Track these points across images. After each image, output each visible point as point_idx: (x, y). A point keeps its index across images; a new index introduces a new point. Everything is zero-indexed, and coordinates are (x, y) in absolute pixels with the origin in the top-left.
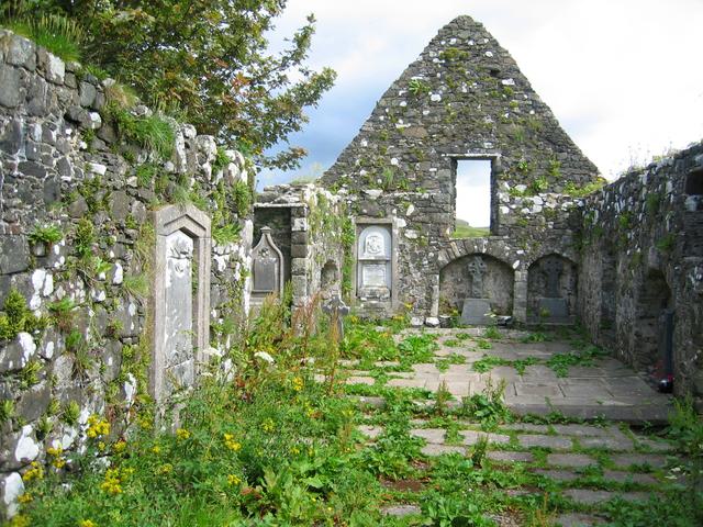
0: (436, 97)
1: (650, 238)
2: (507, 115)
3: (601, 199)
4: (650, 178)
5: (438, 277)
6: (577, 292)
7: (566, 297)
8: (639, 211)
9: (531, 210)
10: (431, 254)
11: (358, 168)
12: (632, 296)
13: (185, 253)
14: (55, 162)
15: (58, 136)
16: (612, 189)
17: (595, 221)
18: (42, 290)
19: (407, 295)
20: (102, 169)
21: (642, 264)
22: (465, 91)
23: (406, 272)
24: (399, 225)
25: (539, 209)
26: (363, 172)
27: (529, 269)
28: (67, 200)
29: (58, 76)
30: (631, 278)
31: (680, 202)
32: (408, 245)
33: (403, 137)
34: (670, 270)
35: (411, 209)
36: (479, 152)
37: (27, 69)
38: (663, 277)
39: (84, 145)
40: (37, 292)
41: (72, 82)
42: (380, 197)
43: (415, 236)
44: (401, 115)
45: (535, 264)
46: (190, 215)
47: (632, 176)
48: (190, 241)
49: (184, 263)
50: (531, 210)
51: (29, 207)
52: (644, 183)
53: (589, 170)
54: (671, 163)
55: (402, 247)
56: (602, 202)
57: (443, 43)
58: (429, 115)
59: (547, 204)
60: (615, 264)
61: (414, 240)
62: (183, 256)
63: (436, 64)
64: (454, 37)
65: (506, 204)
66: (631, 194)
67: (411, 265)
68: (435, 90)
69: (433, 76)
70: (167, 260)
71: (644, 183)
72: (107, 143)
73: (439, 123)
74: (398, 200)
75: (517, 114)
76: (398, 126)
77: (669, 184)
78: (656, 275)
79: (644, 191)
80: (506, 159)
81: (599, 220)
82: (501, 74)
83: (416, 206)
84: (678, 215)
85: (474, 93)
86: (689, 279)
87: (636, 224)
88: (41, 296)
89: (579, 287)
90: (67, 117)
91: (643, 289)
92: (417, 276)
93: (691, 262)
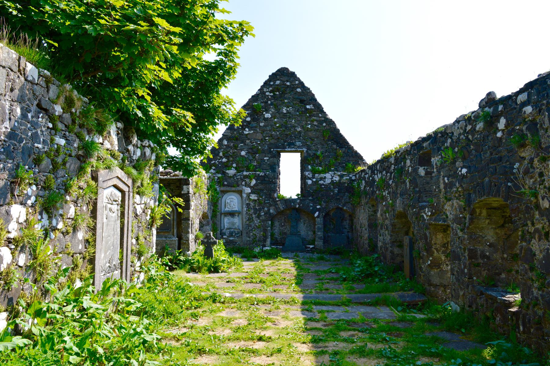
0: (268, 116)
1: (398, 194)
2: (309, 126)
3: (367, 174)
4: (396, 159)
5: (270, 222)
6: (353, 230)
7: (346, 233)
8: (390, 179)
9: (324, 182)
10: (266, 209)
11: (221, 158)
12: (387, 229)
13: (116, 201)
14: (30, 134)
15: (32, 117)
16: (372, 168)
17: (362, 187)
18: (18, 219)
19: (252, 234)
20: (63, 142)
21: (393, 210)
22: (285, 112)
23: (250, 219)
24: (246, 191)
25: (329, 181)
26: (224, 160)
27: (324, 217)
28: (37, 162)
29: (34, 79)
30: (387, 218)
31: (415, 170)
32: (252, 204)
33: (249, 139)
34: (410, 211)
35: (254, 182)
36: (293, 148)
37: (12, 70)
38: (406, 217)
39: (51, 125)
40: (15, 220)
41: (43, 83)
42: (235, 175)
43: (256, 198)
44: (247, 126)
45: (327, 214)
46: (120, 177)
47: (385, 160)
48: (119, 194)
49: (115, 207)
50: (324, 182)
51: (11, 161)
52: (393, 162)
53: (357, 158)
54: (409, 149)
55: (248, 205)
56: (367, 176)
57: (272, 83)
58: (264, 126)
59: (334, 178)
60: (375, 212)
61: (255, 200)
62: (114, 203)
63: (268, 96)
64: (278, 80)
65: (309, 179)
66: (384, 169)
67: (254, 216)
68: (267, 111)
69: (266, 102)
70: (105, 204)
71: (393, 162)
72: (66, 126)
73: (270, 131)
74: (246, 177)
75: (315, 125)
76: (245, 132)
77: (408, 162)
78: (402, 216)
79: (393, 166)
80: (310, 152)
81: (365, 187)
82: (306, 102)
83: (256, 180)
84: (414, 178)
85: (290, 113)
86: (423, 216)
87: (388, 186)
88: (18, 222)
89: (354, 227)
90: (39, 105)
91: (394, 225)
92: (257, 222)
93: (424, 206)
